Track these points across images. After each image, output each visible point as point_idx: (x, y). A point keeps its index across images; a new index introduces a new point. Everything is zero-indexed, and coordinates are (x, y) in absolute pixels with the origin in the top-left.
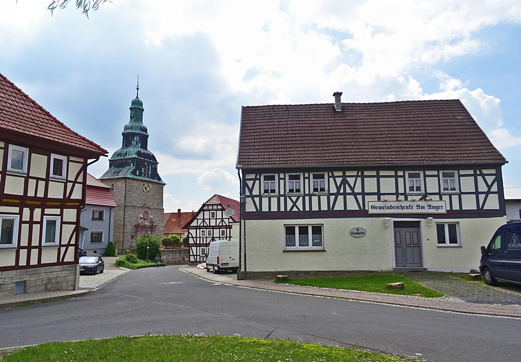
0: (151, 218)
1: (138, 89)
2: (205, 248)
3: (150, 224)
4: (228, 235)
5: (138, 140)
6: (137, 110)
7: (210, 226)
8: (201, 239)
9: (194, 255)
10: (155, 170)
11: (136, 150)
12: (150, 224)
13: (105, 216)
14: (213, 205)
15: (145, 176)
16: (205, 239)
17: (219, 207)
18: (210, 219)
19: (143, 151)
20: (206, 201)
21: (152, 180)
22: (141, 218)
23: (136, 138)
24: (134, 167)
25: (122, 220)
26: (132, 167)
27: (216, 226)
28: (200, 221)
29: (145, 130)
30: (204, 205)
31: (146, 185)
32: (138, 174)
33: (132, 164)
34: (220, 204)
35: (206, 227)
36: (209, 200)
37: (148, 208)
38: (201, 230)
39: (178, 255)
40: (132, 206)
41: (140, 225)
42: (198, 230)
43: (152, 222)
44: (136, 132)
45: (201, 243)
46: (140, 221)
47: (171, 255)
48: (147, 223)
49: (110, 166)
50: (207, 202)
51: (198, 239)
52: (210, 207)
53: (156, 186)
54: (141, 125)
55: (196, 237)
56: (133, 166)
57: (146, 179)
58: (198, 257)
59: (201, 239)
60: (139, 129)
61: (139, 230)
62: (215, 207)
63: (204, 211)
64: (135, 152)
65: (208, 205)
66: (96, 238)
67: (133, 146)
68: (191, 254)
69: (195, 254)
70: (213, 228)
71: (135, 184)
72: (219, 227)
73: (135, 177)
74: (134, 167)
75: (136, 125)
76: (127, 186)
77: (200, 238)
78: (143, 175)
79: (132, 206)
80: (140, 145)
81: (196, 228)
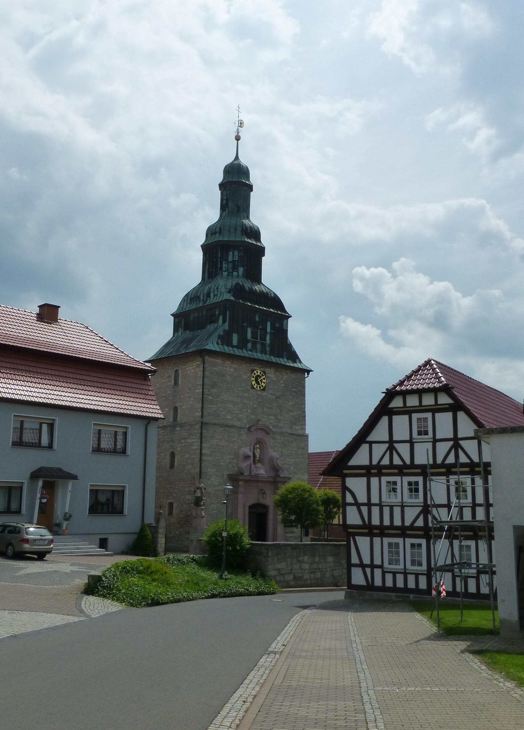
0: (272, 459)
1: (238, 138)
2: (400, 541)
3: (272, 474)
4: (480, 499)
5: (236, 258)
6: (236, 186)
7: (413, 465)
8: (386, 511)
9: (362, 566)
10: (281, 333)
11: (231, 283)
12: (272, 474)
13: (134, 445)
14: (420, 392)
15: (254, 344)
16: (397, 511)
17: (444, 399)
18: (411, 442)
19: (247, 285)
20: (396, 381)
21: (274, 359)
22: (247, 457)
23: (233, 256)
24: (227, 324)
25: (197, 461)
26: (222, 326)
27: (435, 465)
28: (379, 450)
29: (255, 234)
30: (390, 394)
31: (258, 372)
32: (235, 342)
33: (221, 318)
34: (446, 389)
35: (402, 470)
36: (408, 378)
37: (266, 431)
38: (384, 479)
39: (330, 559)
40: (222, 425)
41: (242, 474)
42: (374, 481)
43: (276, 469)
44: (232, 239)
45: (387, 522)
46: (244, 465)
47: (306, 558)
48: (262, 471)
49: (176, 330)
50: (401, 383)
51: (375, 511)
52: (412, 401)
53: (286, 376)
54: (246, 222)
55: (369, 504)
56: (224, 321)
57: (258, 355)
58: (378, 572)
59: (386, 511)
60: (239, 233)
61: (241, 489)
62: (428, 400)
63: (391, 413)
64: (229, 286)
65: (405, 394)
66: (105, 503)
67: (225, 274)
68: (355, 560)
69: (367, 560)
70: (424, 471)
71: (230, 368)
72: (448, 470)
73: (227, 350)
74: (227, 324)
75: (233, 222)
76: (207, 374)
77: (381, 506)
78: (249, 346)
79: (222, 425)
80: (241, 270)
81: (370, 471)
